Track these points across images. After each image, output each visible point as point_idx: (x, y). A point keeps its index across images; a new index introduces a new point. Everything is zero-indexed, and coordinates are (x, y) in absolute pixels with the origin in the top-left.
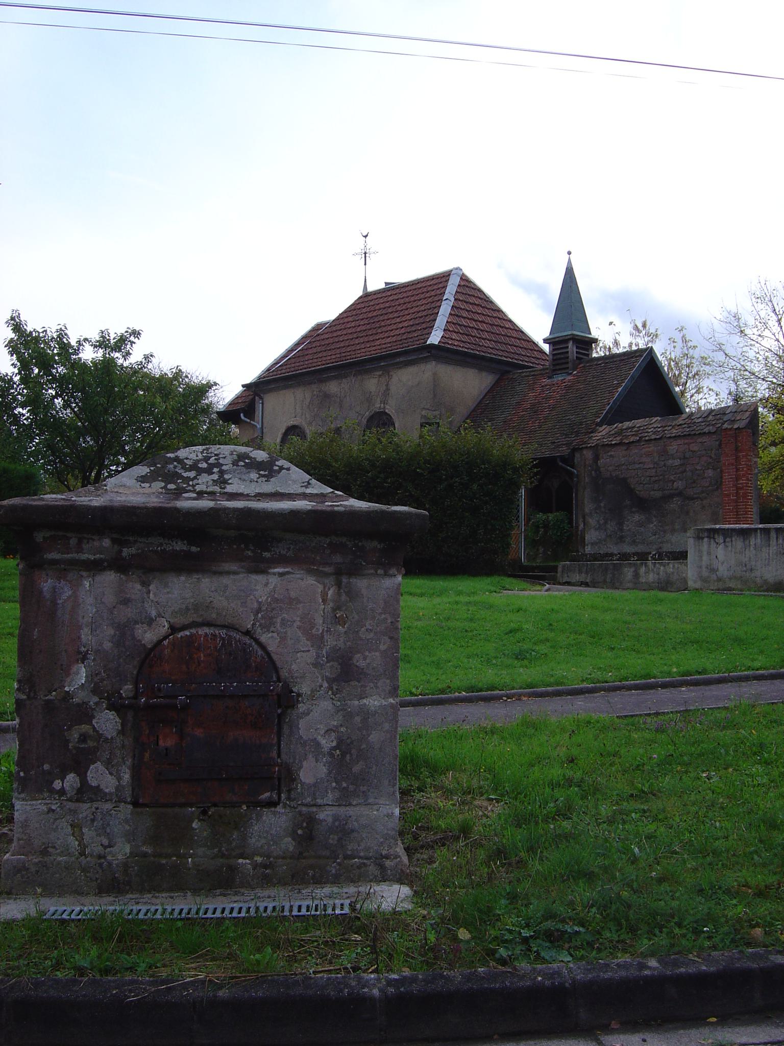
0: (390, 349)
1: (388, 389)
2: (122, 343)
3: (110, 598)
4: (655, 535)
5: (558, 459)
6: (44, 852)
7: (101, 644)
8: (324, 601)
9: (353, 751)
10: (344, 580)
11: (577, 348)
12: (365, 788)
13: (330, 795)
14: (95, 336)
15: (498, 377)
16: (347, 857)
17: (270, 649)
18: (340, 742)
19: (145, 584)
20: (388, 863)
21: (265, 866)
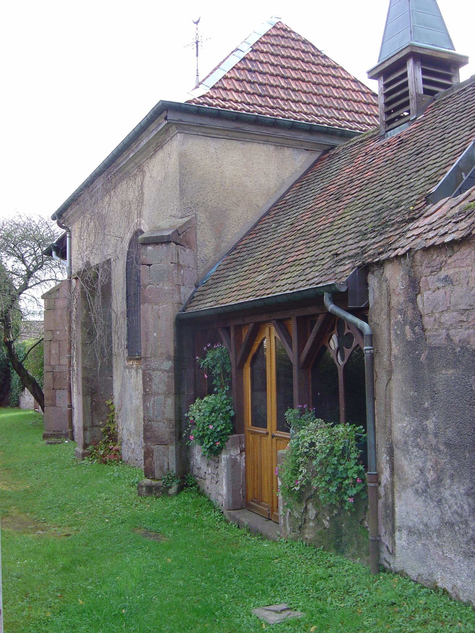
11: (424, 72)
15: (316, 156)
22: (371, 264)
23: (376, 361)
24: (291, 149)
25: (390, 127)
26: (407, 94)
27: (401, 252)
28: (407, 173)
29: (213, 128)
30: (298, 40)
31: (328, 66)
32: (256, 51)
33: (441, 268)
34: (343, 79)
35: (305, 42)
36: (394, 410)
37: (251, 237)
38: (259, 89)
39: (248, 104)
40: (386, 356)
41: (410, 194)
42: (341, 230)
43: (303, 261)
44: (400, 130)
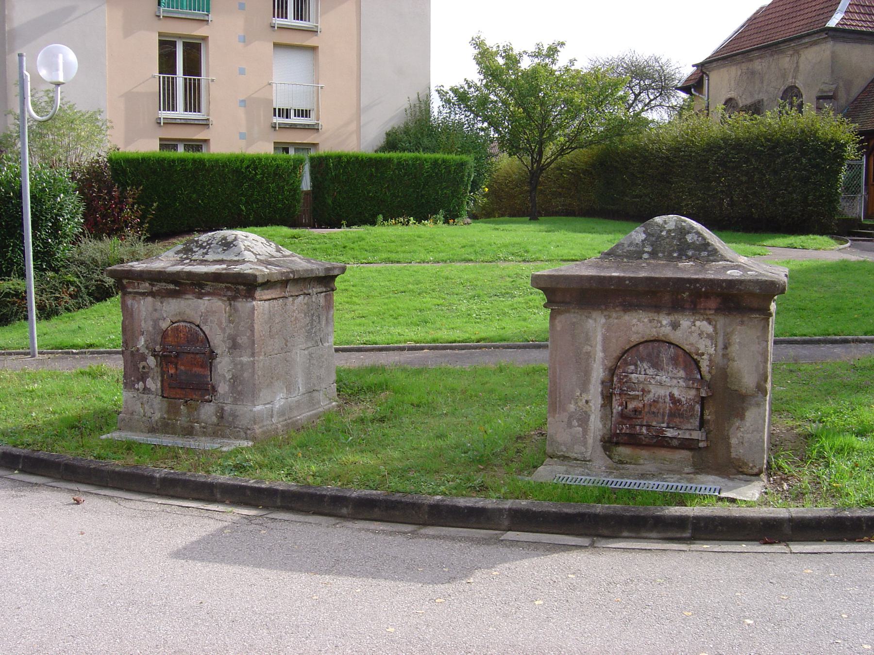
0: (738, 48)
1: (797, 66)
2: (553, 51)
3: (150, 309)
6: (132, 414)
7: (148, 328)
8: (225, 312)
9: (238, 381)
10: (232, 303)
12: (242, 398)
13: (230, 400)
14: (532, 49)
16: (235, 428)
17: (206, 333)
18: (233, 376)
19: (162, 303)
20: (249, 432)
21: (204, 428)
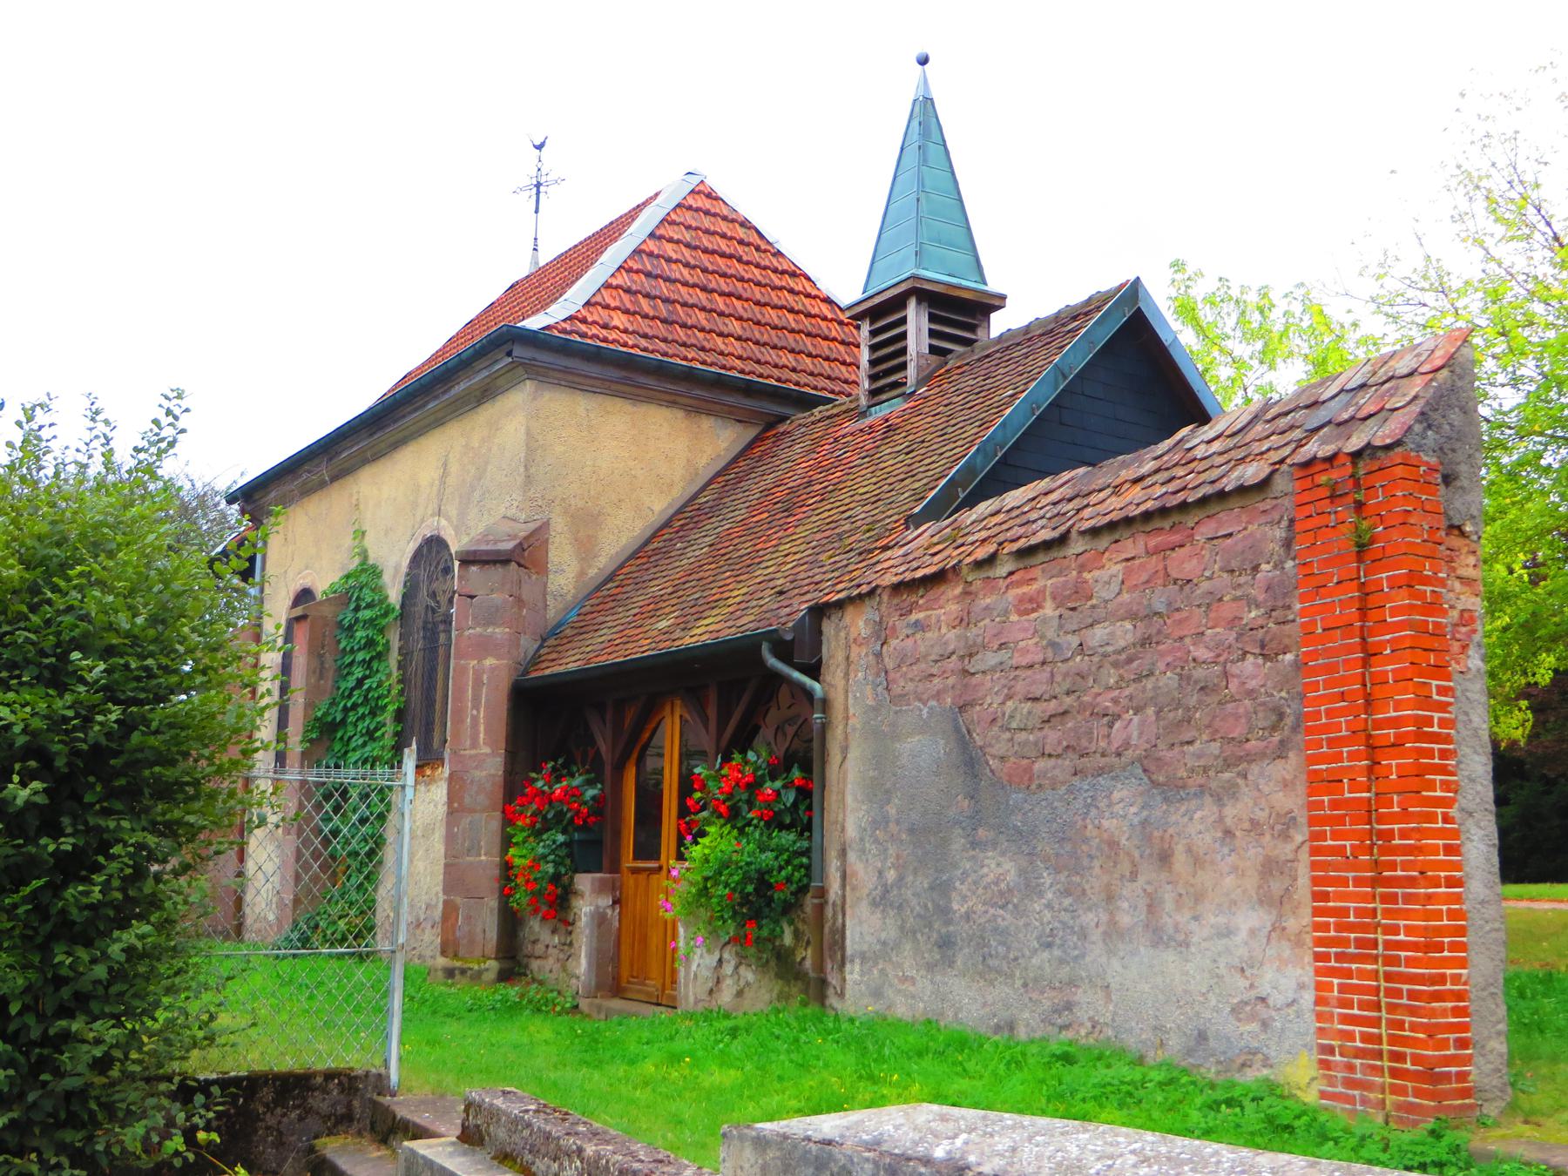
4: (1049, 945)
5: (765, 647)
11: (933, 318)
15: (751, 433)
22: (828, 605)
23: (829, 736)
24: (712, 419)
25: (876, 399)
26: (903, 351)
27: (865, 589)
28: (889, 481)
29: (586, 376)
30: (733, 221)
31: (783, 272)
32: (661, 237)
33: (911, 611)
34: (808, 296)
35: (745, 224)
36: (849, 799)
37: (639, 561)
38: (663, 310)
39: (645, 336)
40: (841, 727)
41: (889, 513)
42: (789, 559)
43: (731, 601)
44: (891, 406)
